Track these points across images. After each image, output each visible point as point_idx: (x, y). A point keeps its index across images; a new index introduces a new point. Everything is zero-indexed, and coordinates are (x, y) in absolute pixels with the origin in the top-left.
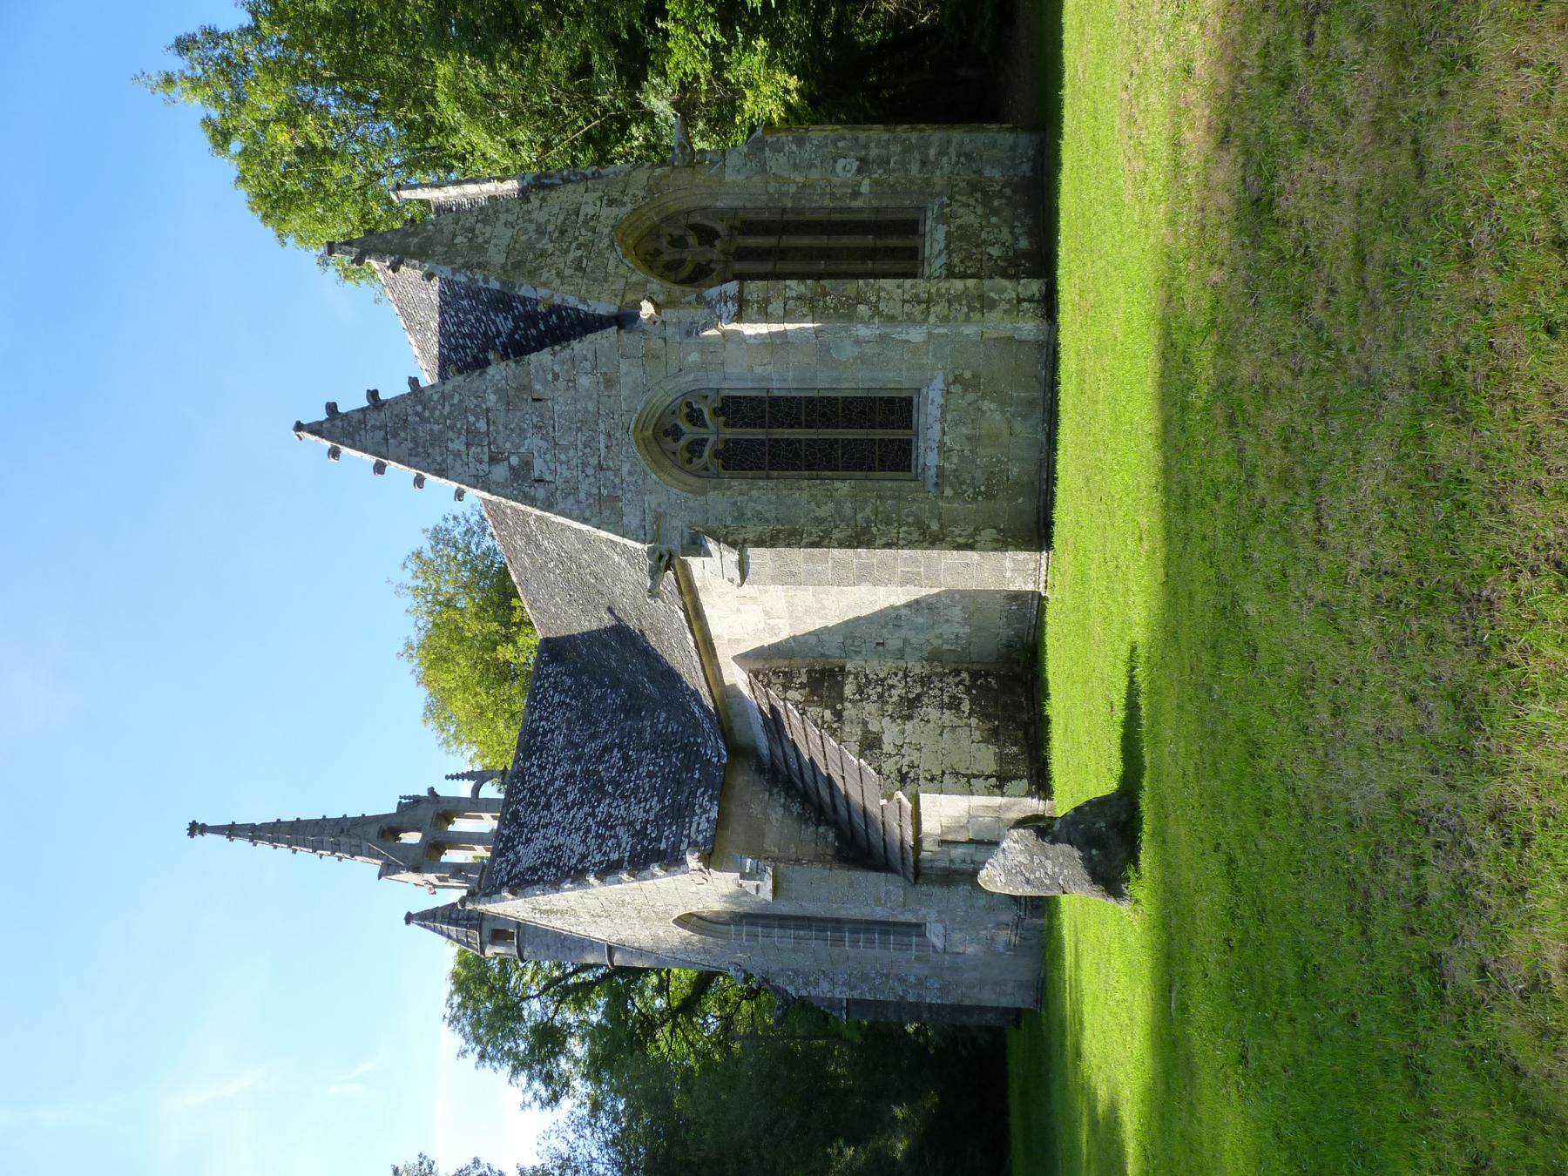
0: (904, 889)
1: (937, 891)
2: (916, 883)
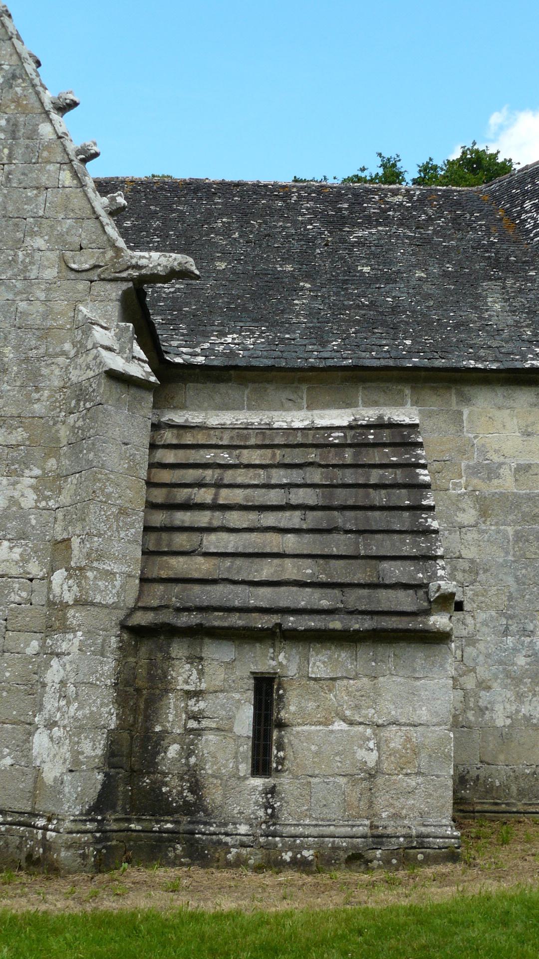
0: (115, 606)
1: (109, 666)
2: (124, 627)
